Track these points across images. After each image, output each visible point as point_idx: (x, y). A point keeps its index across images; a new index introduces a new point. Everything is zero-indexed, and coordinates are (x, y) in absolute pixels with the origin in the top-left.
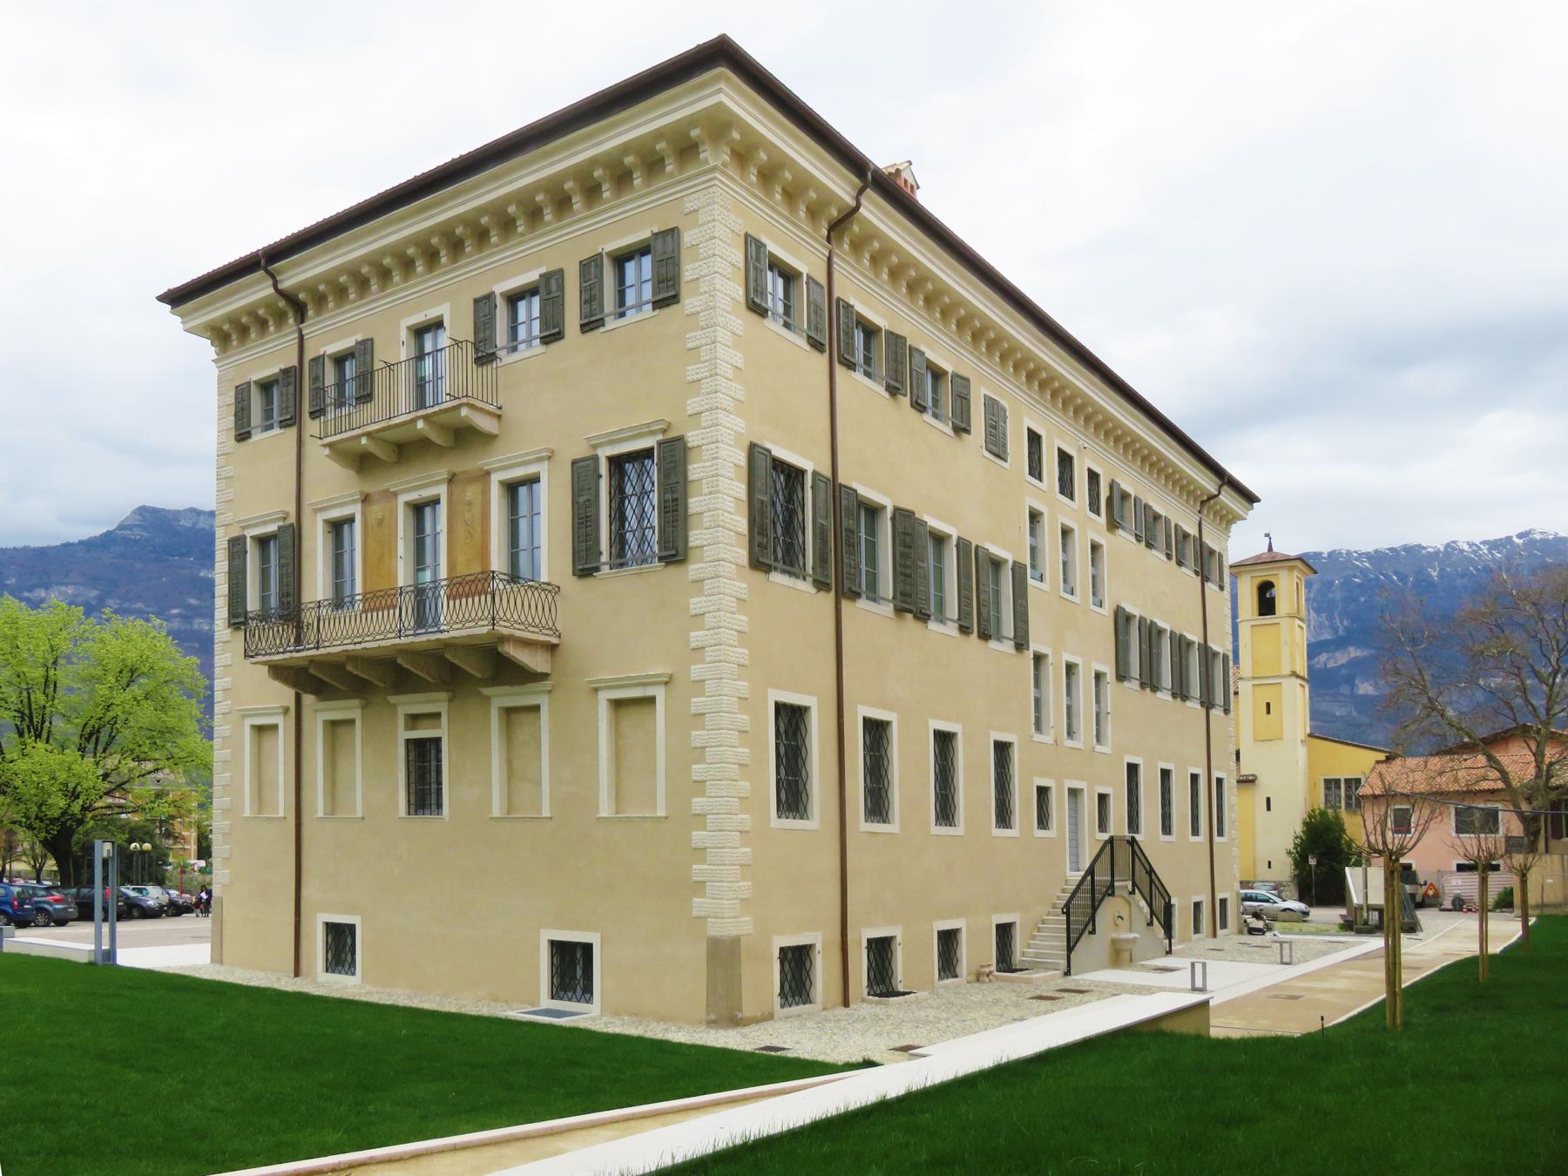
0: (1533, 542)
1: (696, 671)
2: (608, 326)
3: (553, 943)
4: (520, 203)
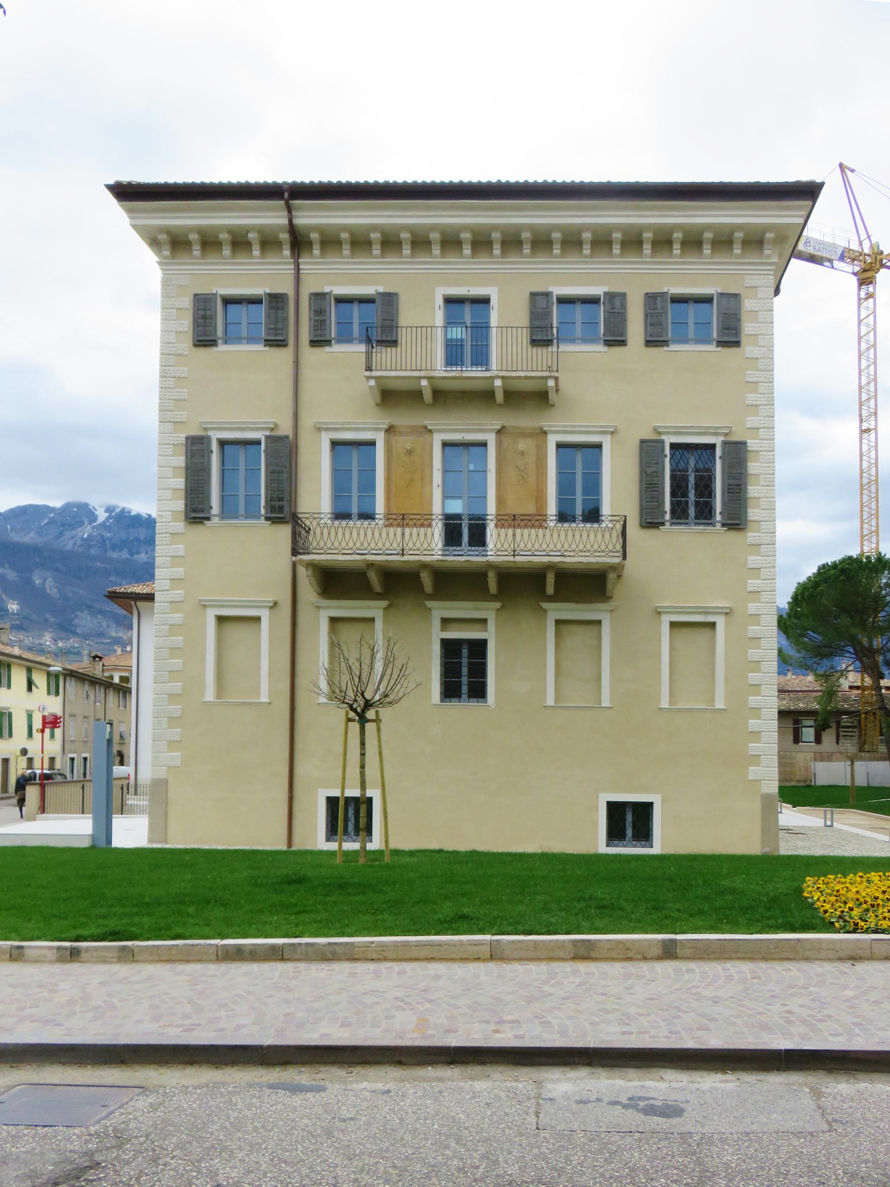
1: (752, 608)
3: (651, 805)
4: (413, 233)
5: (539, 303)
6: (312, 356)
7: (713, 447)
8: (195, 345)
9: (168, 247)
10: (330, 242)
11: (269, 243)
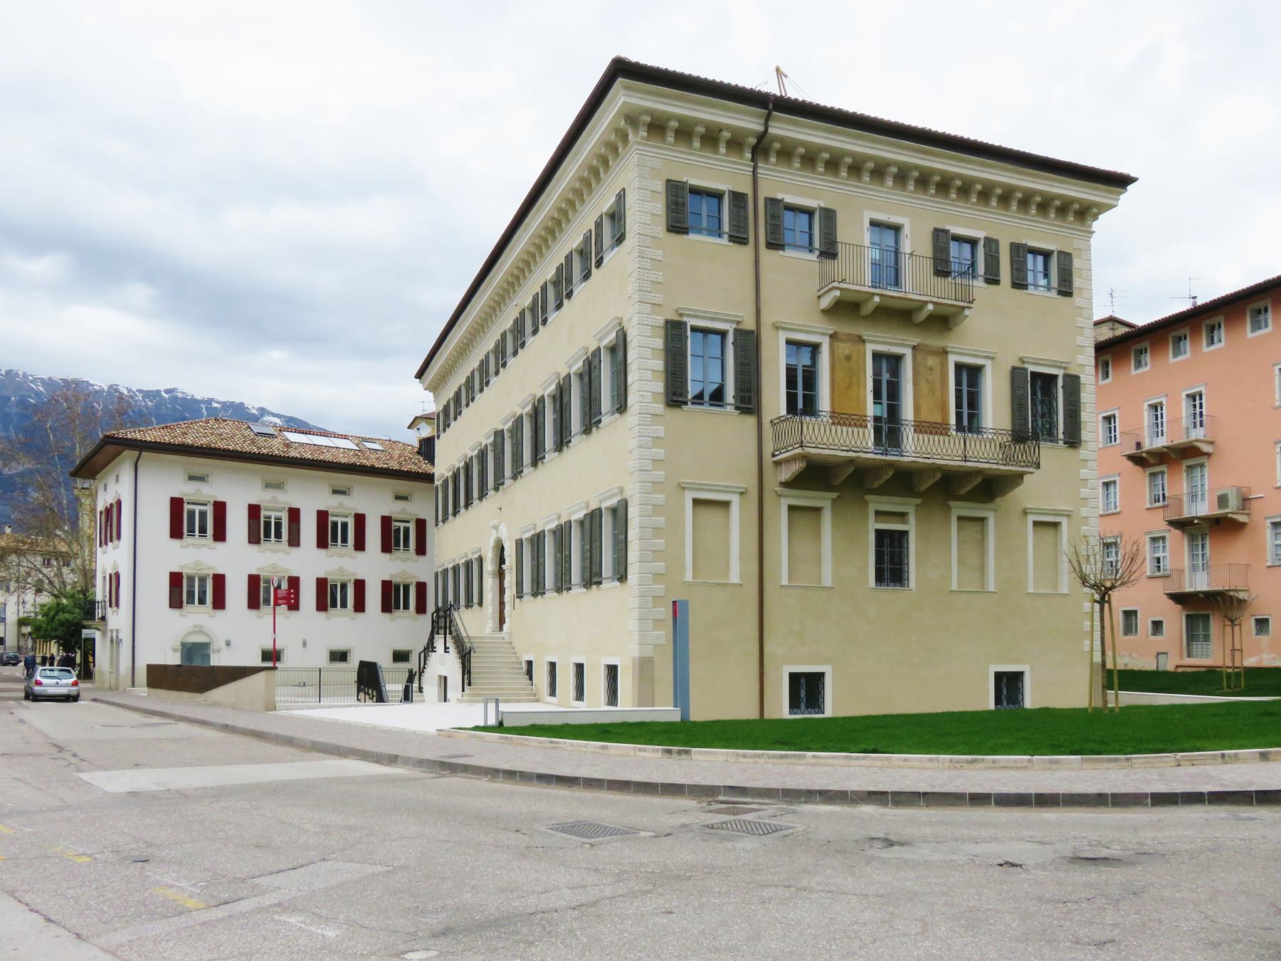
0: (176, 398)
3: (823, 674)
5: (941, 238)
6: (767, 256)
7: (1056, 376)
8: (669, 230)
10: (786, 153)
11: (735, 144)
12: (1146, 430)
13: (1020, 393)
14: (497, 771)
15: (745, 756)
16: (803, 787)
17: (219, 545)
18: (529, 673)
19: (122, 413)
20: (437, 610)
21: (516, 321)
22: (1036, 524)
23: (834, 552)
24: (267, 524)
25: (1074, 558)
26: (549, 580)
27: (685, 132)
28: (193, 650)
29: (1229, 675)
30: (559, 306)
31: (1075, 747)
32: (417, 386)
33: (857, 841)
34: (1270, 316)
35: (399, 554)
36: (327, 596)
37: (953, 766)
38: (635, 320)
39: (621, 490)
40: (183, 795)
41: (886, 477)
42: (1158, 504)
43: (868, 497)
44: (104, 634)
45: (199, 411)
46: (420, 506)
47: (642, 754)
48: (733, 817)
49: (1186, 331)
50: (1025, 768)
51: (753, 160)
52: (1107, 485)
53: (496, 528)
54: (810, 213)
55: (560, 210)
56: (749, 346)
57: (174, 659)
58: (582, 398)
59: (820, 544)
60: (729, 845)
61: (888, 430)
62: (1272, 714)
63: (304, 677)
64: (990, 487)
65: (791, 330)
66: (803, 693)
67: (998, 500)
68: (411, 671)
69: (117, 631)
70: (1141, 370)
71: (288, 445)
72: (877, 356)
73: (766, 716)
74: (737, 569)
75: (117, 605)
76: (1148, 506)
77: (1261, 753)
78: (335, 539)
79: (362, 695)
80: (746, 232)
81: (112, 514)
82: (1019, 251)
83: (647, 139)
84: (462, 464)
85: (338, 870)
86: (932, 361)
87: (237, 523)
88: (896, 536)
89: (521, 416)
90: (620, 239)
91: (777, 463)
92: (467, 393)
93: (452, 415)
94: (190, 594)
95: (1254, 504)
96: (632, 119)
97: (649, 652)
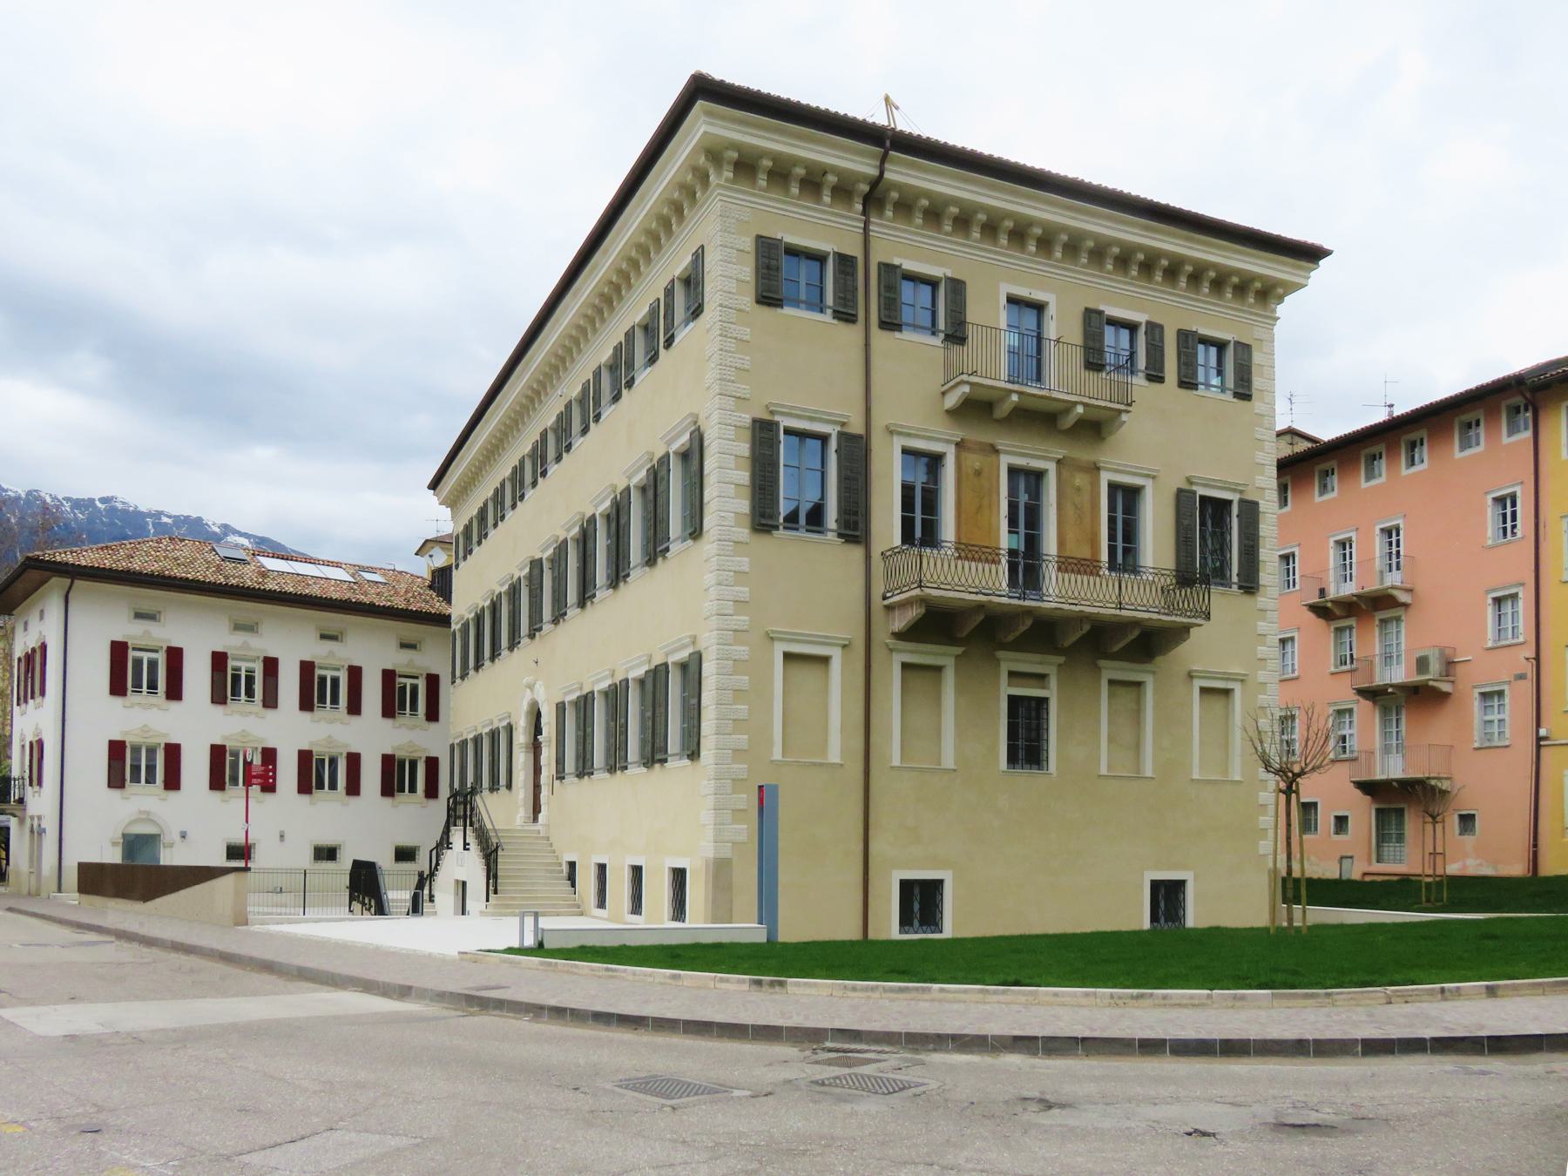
2: (1199, 392)
3: (941, 882)
5: (1094, 321)
6: (880, 338)
7: (1230, 502)
8: (758, 302)
9: (731, 168)
10: (905, 206)
11: (843, 191)
12: (1331, 572)
13: (1186, 522)
14: (541, 1008)
15: (854, 989)
16: (931, 1030)
17: (174, 705)
18: (572, 878)
19: (46, 528)
20: (454, 795)
21: (560, 417)
22: (1204, 691)
23: (957, 725)
24: (236, 678)
25: (1255, 736)
26: (599, 757)
27: (780, 174)
28: (134, 844)
29: (1428, 885)
30: (616, 398)
31: (1263, 979)
32: (431, 498)
33: (1006, 1102)
34: (1482, 430)
35: (404, 720)
36: (312, 773)
37: (1114, 1002)
38: (715, 418)
39: (694, 641)
40: (137, 1039)
41: (1022, 629)
42: (1344, 668)
43: (1001, 654)
44: (22, 821)
45: (144, 527)
46: (433, 658)
47: (724, 986)
48: (846, 1071)
49: (1381, 448)
50: (1202, 1005)
51: (864, 213)
52: (1283, 642)
53: (531, 687)
54: (933, 283)
55: (620, 272)
56: (856, 454)
57: (114, 856)
58: (645, 519)
59: (939, 715)
60: (848, 1107)
61: (1026, 567)
62: (1494, 937)
63: (281, 881)
64: (1149, 642)
65: (909, 435)
66: (916, 906)
67: (1159, 660)
68: (421, 874)
69: (39, 818)
70: (1327, 497)
71: (264, 574)
72: (1013, 471)
73: (871, 936)
74: (838, 746)
75: (40, 783)
76: (1333, 669)
77: (1487, 987)
78: (322, 699)
79: (357, 906)
80: (855, 306)
81: (34, 662)
82: (1187, 340)
83: (734, 181)
84: (487, 603)
85: (351, 1143)
86: (1080, 480)
87: (197, 676)
88: (1033, 704)
89: (565, 541)
90: (696, 312)
91: (889, 608)
92: (495, 509)
93: (475, 539)
94: (136, 769)
95: (1460, 669)
96: (714, 154)
97: (726, 852)
